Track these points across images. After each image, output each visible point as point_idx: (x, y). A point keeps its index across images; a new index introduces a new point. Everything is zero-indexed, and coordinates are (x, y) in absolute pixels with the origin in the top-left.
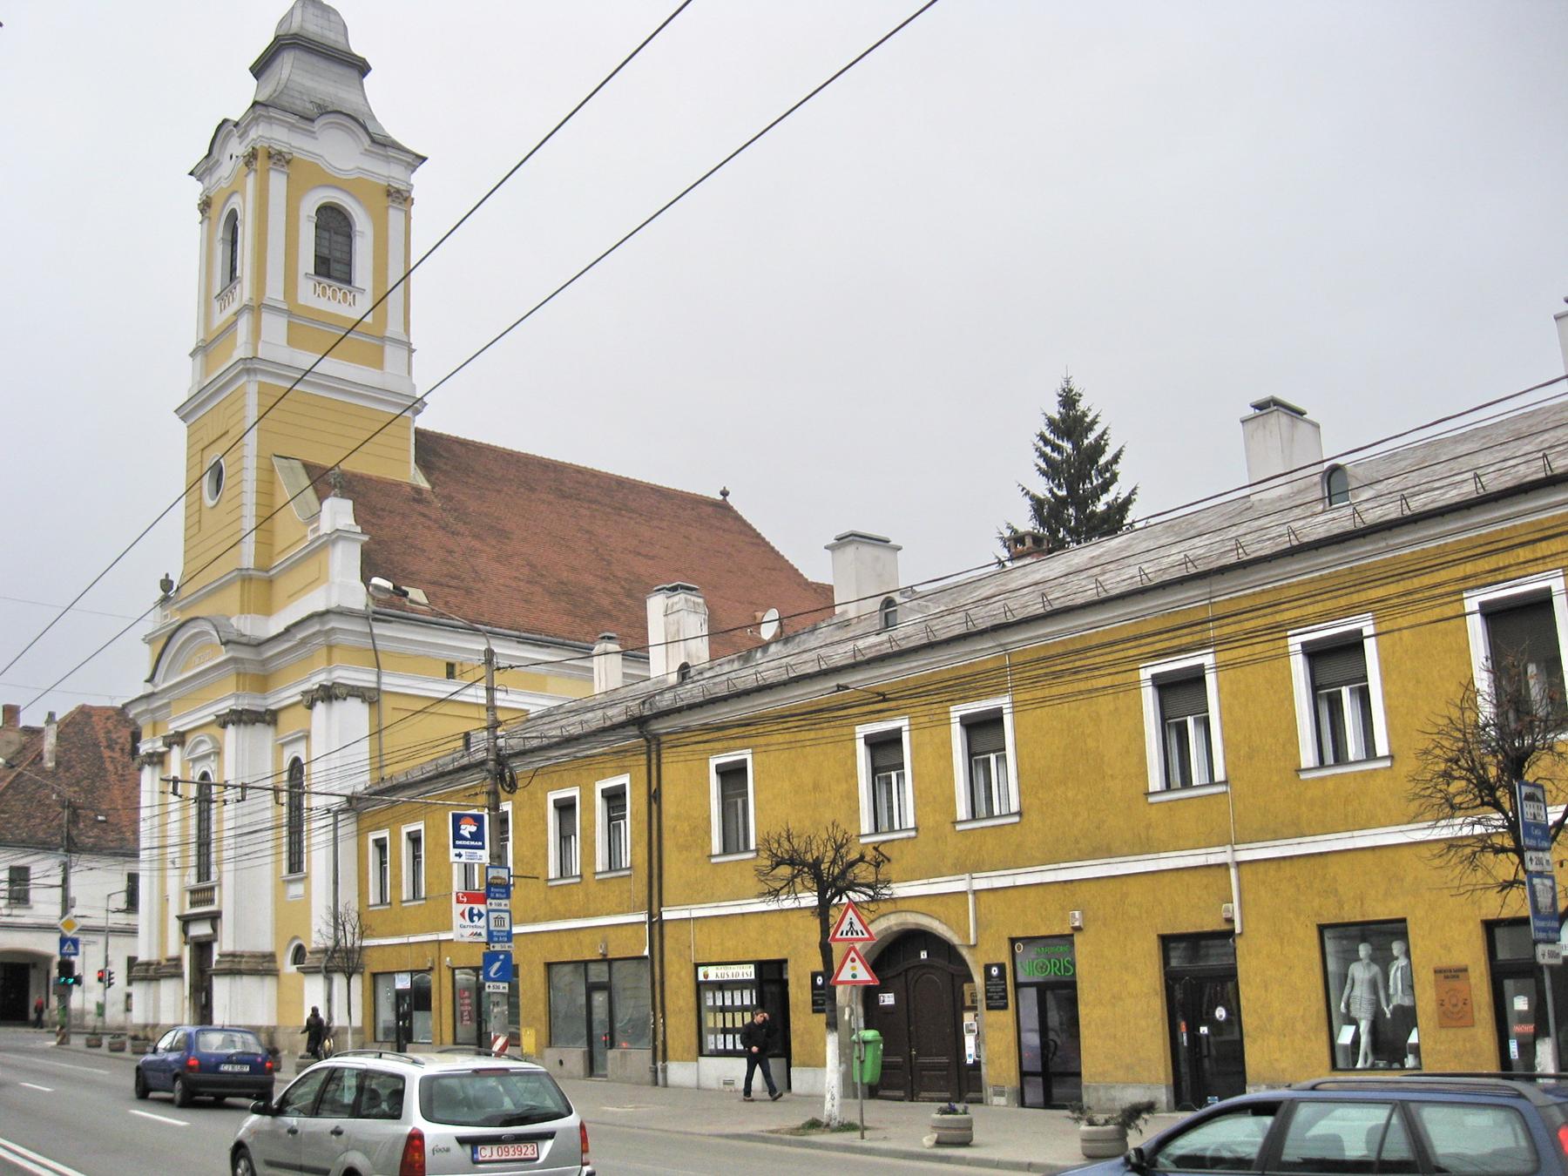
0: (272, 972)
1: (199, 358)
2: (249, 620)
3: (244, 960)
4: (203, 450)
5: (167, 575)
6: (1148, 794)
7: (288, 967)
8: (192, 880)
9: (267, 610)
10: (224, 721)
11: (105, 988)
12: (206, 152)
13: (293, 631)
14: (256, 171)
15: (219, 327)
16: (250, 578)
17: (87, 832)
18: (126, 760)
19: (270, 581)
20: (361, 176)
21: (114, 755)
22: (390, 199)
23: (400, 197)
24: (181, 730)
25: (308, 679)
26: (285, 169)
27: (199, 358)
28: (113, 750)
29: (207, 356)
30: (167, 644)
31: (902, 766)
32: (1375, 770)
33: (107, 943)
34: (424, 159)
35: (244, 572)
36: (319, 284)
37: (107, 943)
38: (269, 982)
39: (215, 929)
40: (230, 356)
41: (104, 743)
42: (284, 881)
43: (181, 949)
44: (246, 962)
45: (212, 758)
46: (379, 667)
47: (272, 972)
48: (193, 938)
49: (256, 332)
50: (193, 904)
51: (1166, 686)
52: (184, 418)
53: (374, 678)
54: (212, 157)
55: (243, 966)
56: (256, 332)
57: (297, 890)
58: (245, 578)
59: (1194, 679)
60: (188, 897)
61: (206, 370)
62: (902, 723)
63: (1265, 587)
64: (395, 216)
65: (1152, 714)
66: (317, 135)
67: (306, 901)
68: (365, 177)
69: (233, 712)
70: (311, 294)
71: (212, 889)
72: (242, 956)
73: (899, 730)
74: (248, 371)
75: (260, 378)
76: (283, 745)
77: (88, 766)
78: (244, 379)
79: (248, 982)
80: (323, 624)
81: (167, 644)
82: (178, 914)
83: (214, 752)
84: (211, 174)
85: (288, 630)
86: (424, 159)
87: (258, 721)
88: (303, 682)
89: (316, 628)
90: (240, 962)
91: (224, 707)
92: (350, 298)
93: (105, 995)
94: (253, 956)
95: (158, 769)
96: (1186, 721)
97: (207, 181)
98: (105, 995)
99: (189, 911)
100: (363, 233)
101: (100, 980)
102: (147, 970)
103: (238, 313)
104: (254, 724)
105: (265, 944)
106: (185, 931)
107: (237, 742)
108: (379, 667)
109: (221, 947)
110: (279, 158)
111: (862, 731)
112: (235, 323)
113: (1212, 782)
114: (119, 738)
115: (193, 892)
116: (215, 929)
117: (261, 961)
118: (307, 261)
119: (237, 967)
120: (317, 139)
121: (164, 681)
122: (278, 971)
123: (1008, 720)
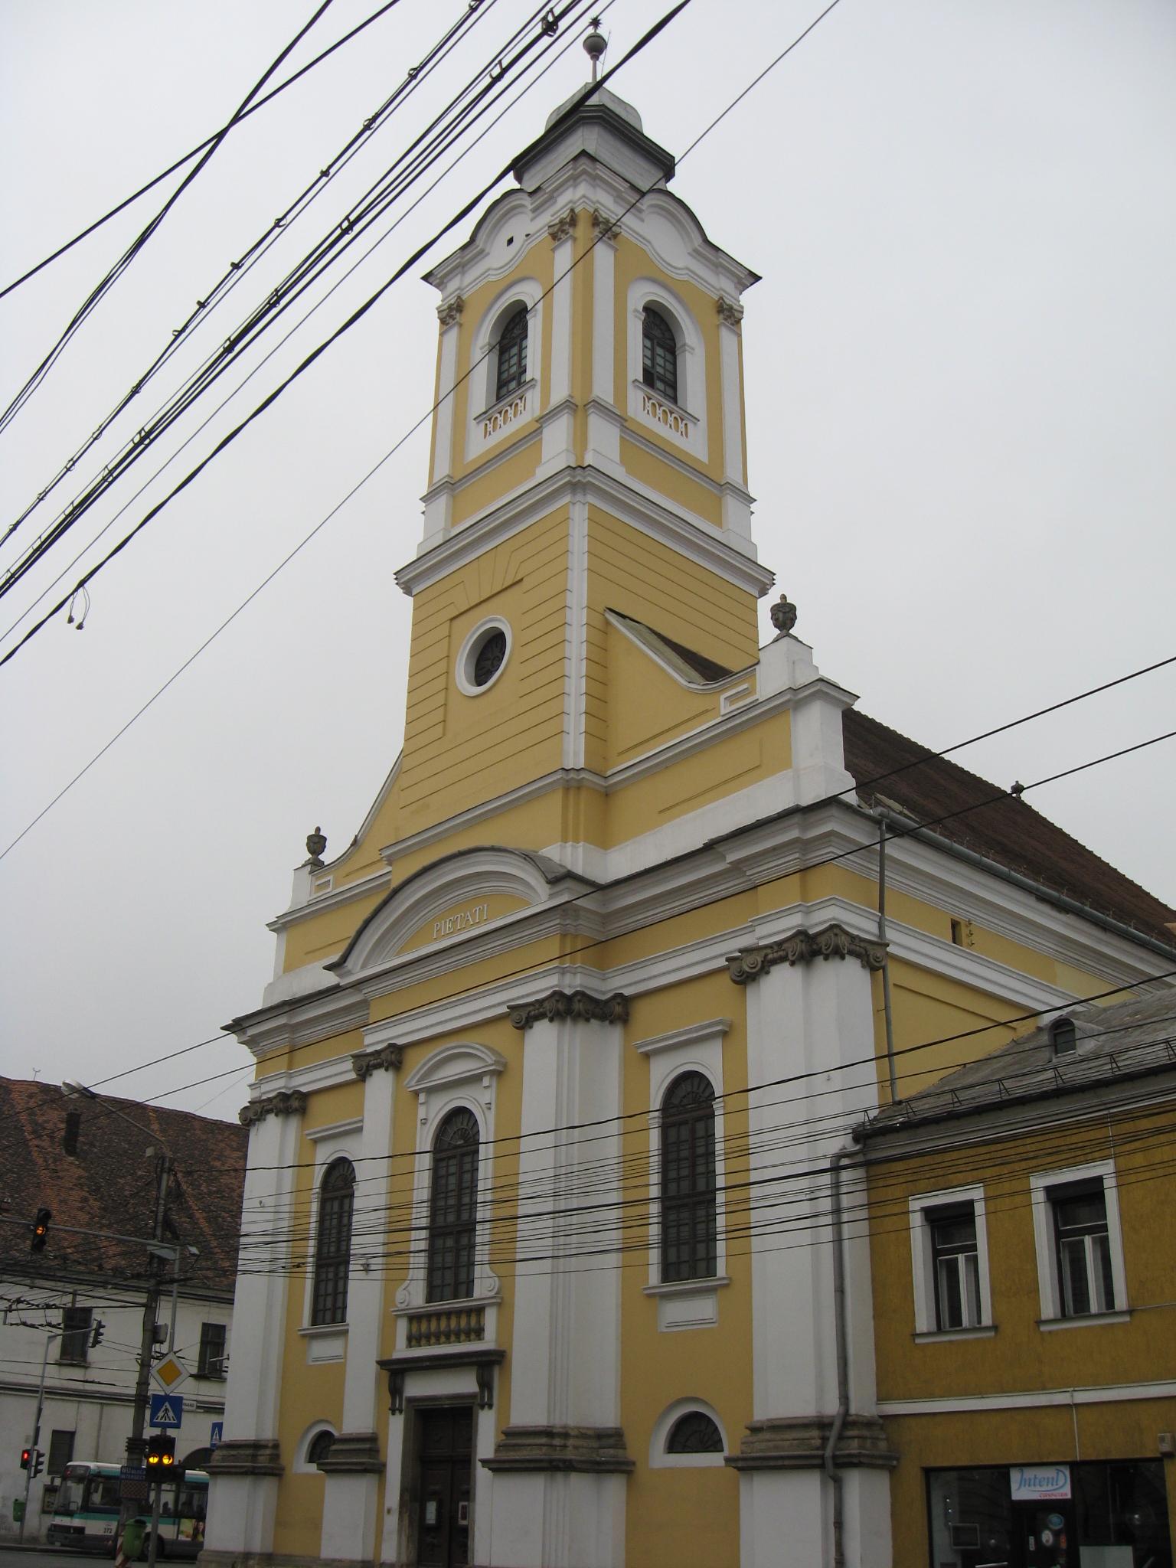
0: (623, 1468)
1: (442, 502)
2: (580, 850)
3: (571, 1442)
4: (452, 619)
5: (318, 829)
6: (915, 1335)
7: (301, 1466)
8: (414, 1293)
9: (604, 839)
10: (524, 1017)
11: (29, 1478)
12: (467, 239)
13: (721, 848)
14: (575, 239)
15: (474, 461)
16: (579, 786)
17: (17, 1244)
18: (57, 1151)
19: (607, 795)
20: (691, 280)
21: (43, 1144)
22: (721, 316)
23: (731, 316)
24: (400, 1042)
25: (750, 929)
26: (612, 242)
27: (442, 502)
28: (40, 1137)
29: (454, 497)
30: (385, 903)
31: (974, 1248)
32: (1113, 1324)
33: (40, 1410)
34: (757, 278)
35: (572, 775)
36: (649, 399)
37: (40, 1410)
38: (614, 1488)
39: (485, 1384)
40: (532, 474)
41: (28, 1128)
42: (304, 1336)
43: (381, 1422)
44: (576, 1447)
45: (486, 1081)
46: (881, 909)
47: (623, 1468)
48: (410, 1400)
49: (580, 440)
50: (413, 1340)
51: (1063, 1200)
52: (408, 591)
53: (873, 928)
54: (473, 247)
55: (570, 1454)
56: (580, 440)
57: (323, 1349)
58: (571, 783)
59: (1092, 1190)
60: (402, 1328)
61: (454, 517)
62: (976, 1193)
63: (1112, 1111)
64: (726, 336)
65: (307, 1318)
66: (643, 215)
67: (336, 1371)
68: (693, 282)
69: (557, 995)
70: (637, 404)
71: (480, 1310)
72: (565, 1435)
73: (1099, 1180)
74: (574, 487)
75: (591, 499)
76: (316, 1141)
77: (12, 1155)
78: (567, 499)
79: (579, 1485)
80: (805, 828)
81: (385, 903)
82: (378, 1359)
83: (492, 1073)
84: (463, 273)
85: (710, 847)
86: (757, 278)
87: (595, 1016)
88: (735, 934)
89: (794, 834)
90: (565, 1446)
91: (538, 988)
92: (682, 426)
93: (27, 1489)
94: (583, 1434)
95: (294, 1123)
96: (1082, 1242)
97: (453, 285)
98: (27, 1489)
99: (401, 1350)
100: (693, 349)
101: (25, 1464)
102: (254, 1457)
103: (543, 420)
104: (588, 1020)
105: (605, 1414)
106: (396, 1390)
107: (560, 1052)
108: (881, 909)
109: (504, 1414)
110: (606, 230)
111: (1039, 1182)
112: (538, 431)
113: (978, 1328)
114: (45, 1121)
115: (414, 1318)
116: (485, 1384)
117: (595, 1444)
118: (636, 372)
119: (557, 1455)
120: (642, 220)
121: (364, 967)
122: (283, 1469)
123: (1111, 1197)
